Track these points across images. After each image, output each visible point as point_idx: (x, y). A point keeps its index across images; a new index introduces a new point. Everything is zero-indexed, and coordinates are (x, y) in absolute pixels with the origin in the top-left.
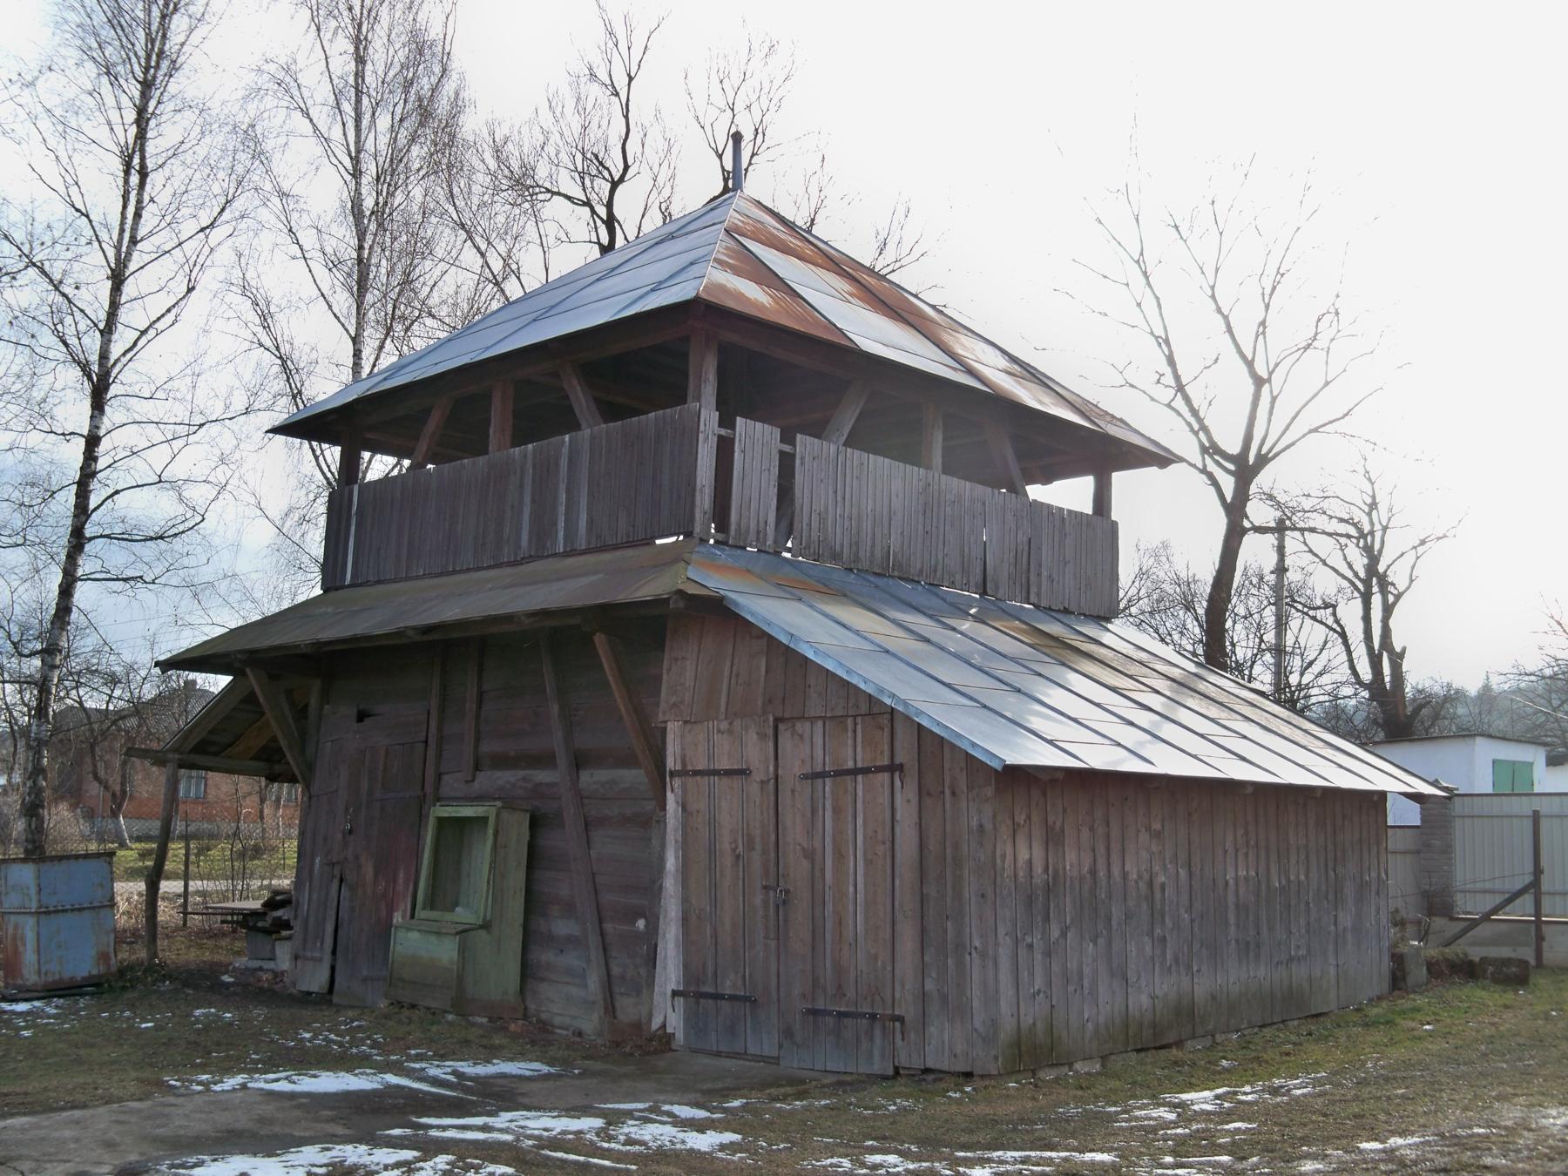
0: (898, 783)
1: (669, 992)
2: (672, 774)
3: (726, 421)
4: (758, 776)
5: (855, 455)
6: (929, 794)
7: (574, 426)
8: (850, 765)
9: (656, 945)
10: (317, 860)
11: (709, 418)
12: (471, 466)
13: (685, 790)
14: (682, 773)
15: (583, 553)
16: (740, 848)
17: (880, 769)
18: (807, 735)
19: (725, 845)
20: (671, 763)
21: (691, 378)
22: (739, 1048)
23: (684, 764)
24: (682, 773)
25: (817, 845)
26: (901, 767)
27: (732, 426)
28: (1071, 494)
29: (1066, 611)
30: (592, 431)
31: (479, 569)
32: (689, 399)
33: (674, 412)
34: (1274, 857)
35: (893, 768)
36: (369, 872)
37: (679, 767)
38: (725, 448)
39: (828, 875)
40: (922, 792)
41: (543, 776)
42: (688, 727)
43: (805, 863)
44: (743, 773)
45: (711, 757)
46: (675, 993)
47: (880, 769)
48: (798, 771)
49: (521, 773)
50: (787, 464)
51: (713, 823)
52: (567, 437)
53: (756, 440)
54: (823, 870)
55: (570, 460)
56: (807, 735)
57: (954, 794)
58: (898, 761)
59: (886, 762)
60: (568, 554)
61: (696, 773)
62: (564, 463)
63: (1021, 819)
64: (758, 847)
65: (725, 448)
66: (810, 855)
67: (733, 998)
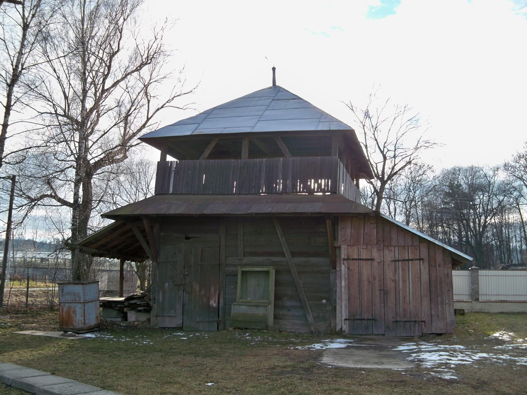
2: (344, 259)
14: (348, 259)
17: (416, 260)
18: (393, 250)
23: (348, 256)
24: (348, 259)
26: (423, 259)
36: (197, 288)
43: (393, 284)
44: (372, 260)
46: (345, 319)
47: (416, 260)
48: (390, 259)
49: (265, 258)
51: (360, 273)
54: (399, 285)
57: (439, 266)
58: (422, 258)
59: (418, 258)
64: (377, 279)
66: (394, 281)
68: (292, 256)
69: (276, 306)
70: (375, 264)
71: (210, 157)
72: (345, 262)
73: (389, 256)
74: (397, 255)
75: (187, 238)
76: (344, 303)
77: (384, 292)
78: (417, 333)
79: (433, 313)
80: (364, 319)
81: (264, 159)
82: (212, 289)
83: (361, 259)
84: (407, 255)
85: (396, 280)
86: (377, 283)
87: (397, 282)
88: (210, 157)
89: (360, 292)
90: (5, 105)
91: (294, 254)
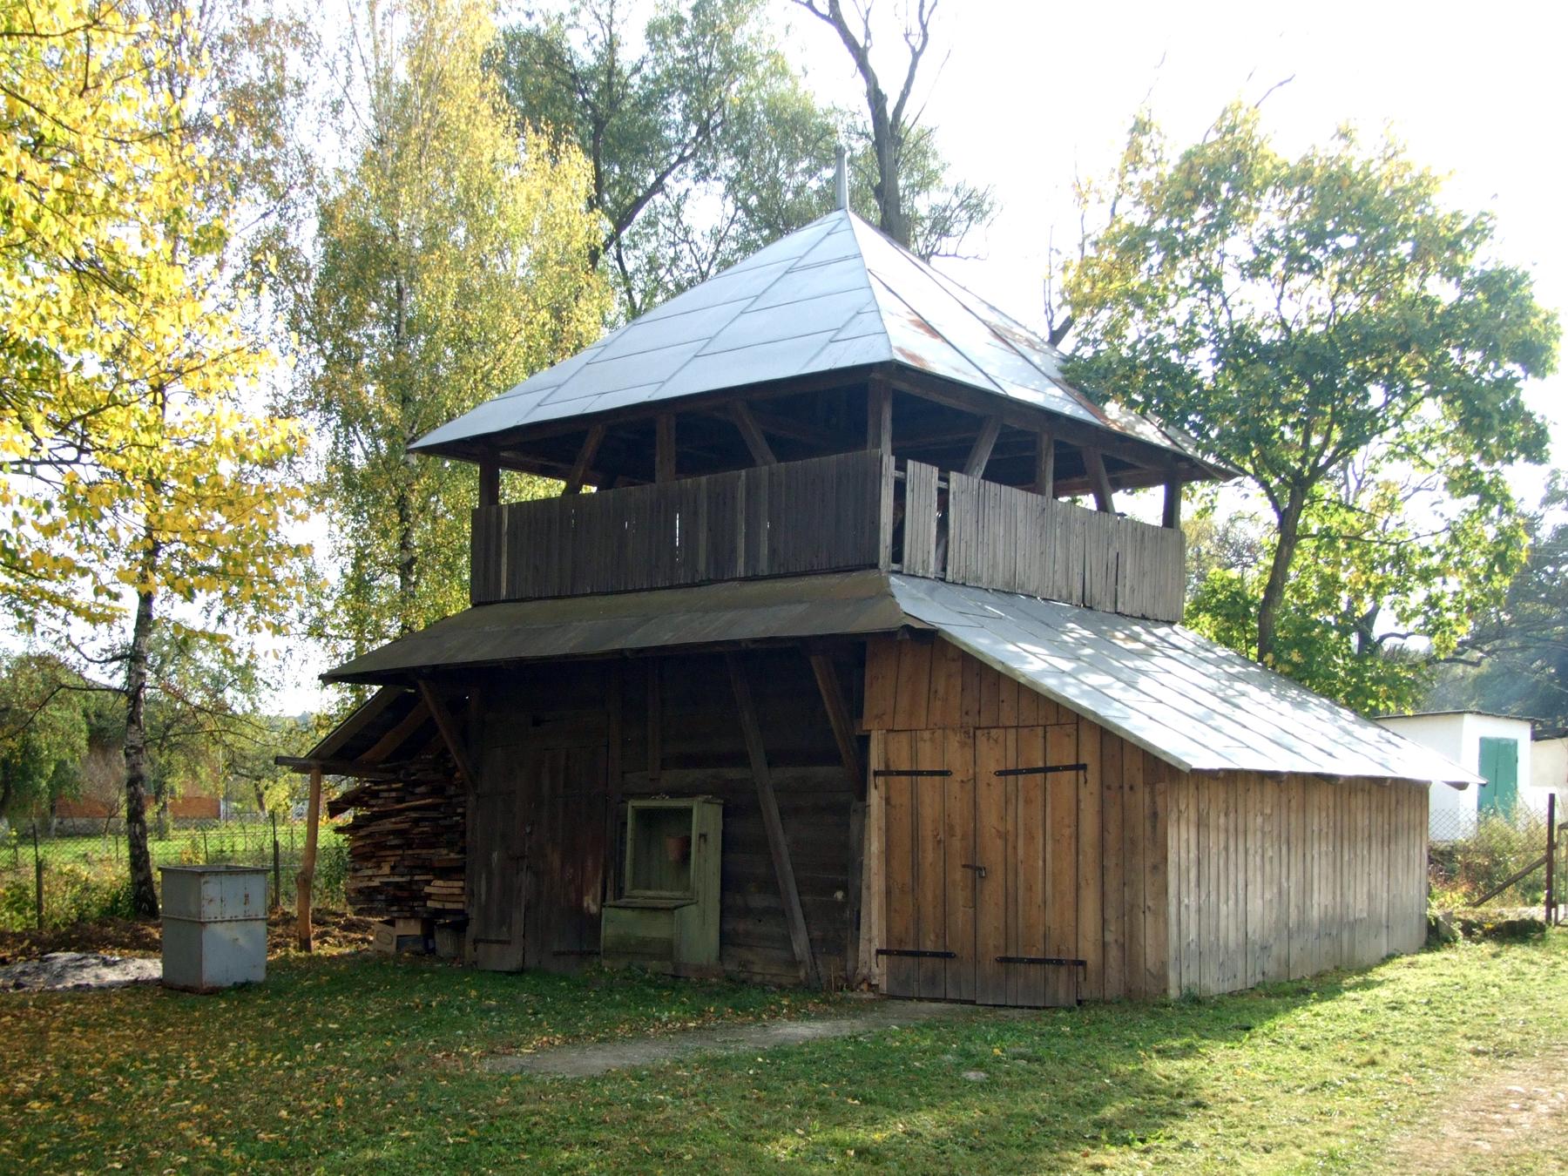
0: (1082, 779)
1: (873, 952)
2: (876, 774)
3: (901, 467)
4: (958, 777)
5: (993, 487)
6: (1109, 788)
7: (747, 461)
8: (1040, 764)
9: (859, 913)
10: (495, 855)
11: (889, 461)
12: (638, 494)
13: (888, 788)
14: (887, 773)
15: (764, 578)
16: (941, 836)
17: (1067, 768)
18: (1001, 739)
19: (927, 830)
20: (875, 763)
21: (870, 422)
22: (939, 994)
23: (887, 765)
24: (887, 773)
25: (1010, 827)
26: (1084, 767)
27: (947, 480)
28: (1142, 505)
29: (1144, 617)
30: (768, 468)
31: (652, 589)
32: (869, 444)
33: (860, 453)
34: (1346, 843)
35: (1079, 767)
36: (556, 859)
37: (882, 768)
38: (900, 488)
39: (1021, 852)
40: (1104, 786)
41: (822, 772)
42: (891, 735)
43: (999, 843)
44: (944, 773)
45: (914, 755)
46: (879, 952)
47: (1067, 768)
48: (993, 767)
49: (710, 771)
50: (943, 494)
51: (915, 814)
52: (743, 472)
53: (922, 476)
54: (1015, 848)
55: (748, 493)
56: (1001, 739)
57: (1131, 788)
58: (1081, 762)
59: (1073, 762)
60: (746, 579)
61: (900, 773)
62: (741, 494)
63: (1183, 807)
64: (958, 832)
65: (900, 488)
66: (1003, 836)
67: (934, 955)
68: (769, 764)
69: (725, 911)
70: (953, 784)
71: (1103, 456)
72: (880, 780)
73: (991, 757)
74: (1011, 753)
75: (537, 722)
76: (929, 896)
77: (977, 871)
78: (1063, 995)
79: (1110, 937)
80: (924, 954)
81: (704, 479)
82: (590, 863)
83: (920, 773)
84: (1040, 754)
85: (1007, 832)
86: (957, 844)
87: (1011, 839)
88: (1103, 456)
89: (916, 867)
90: (1055, 328)
91: (773, 760)
